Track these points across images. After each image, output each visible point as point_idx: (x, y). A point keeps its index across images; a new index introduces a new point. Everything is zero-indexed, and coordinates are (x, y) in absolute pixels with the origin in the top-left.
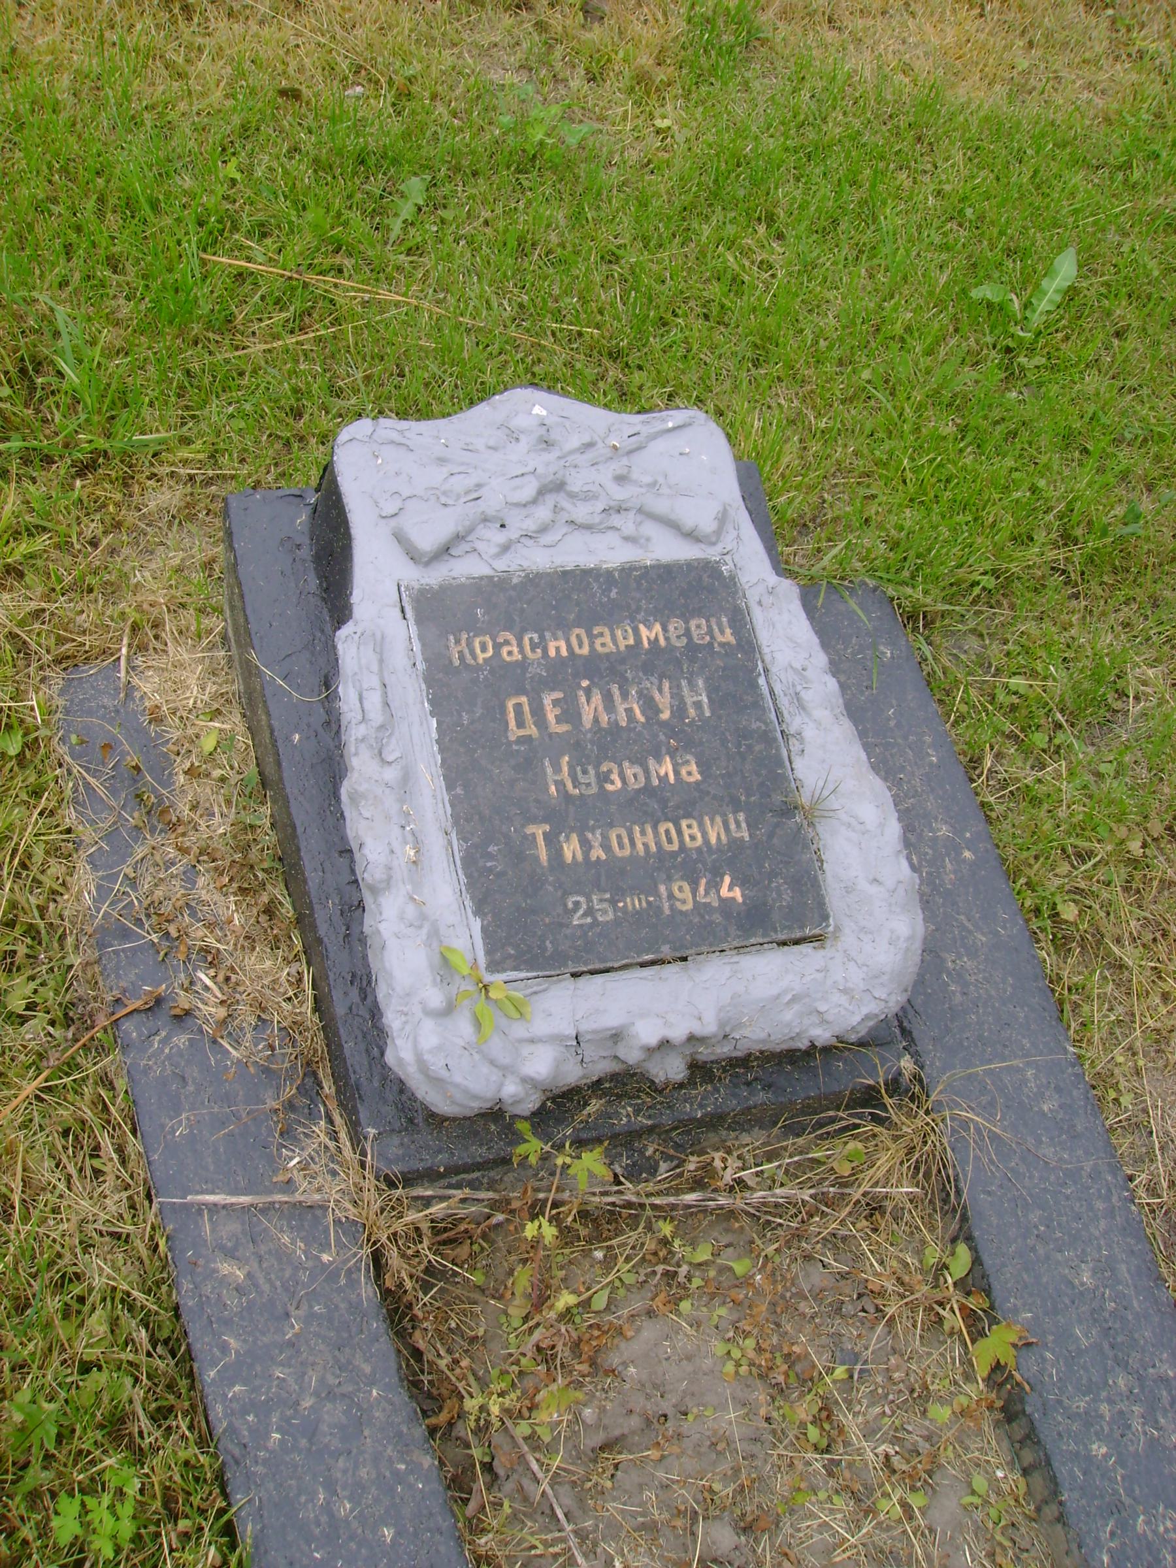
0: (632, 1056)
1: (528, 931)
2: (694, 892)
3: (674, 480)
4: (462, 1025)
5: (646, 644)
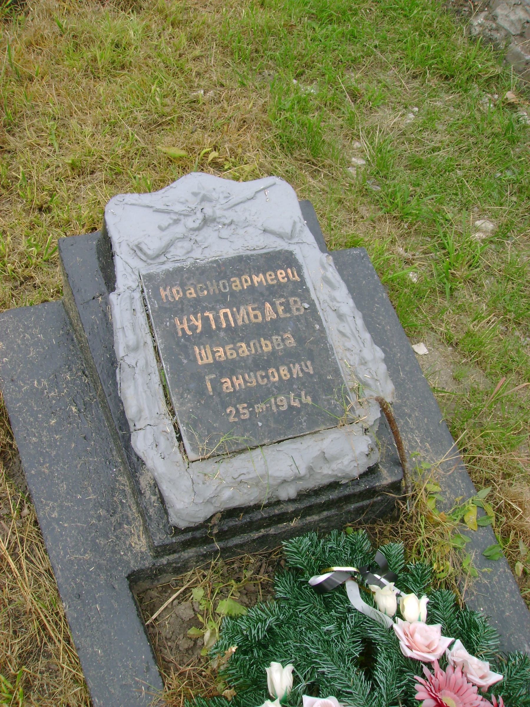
2: (288, 399)
3: (266, 210)
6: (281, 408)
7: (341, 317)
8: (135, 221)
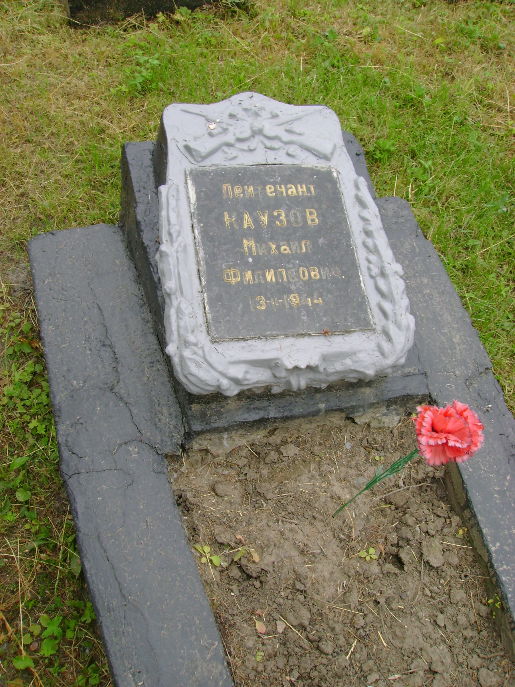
1: (230, 316)
3: (318, 132)
4: (214, 359)
7: (368, 233)
8: (182, 122)
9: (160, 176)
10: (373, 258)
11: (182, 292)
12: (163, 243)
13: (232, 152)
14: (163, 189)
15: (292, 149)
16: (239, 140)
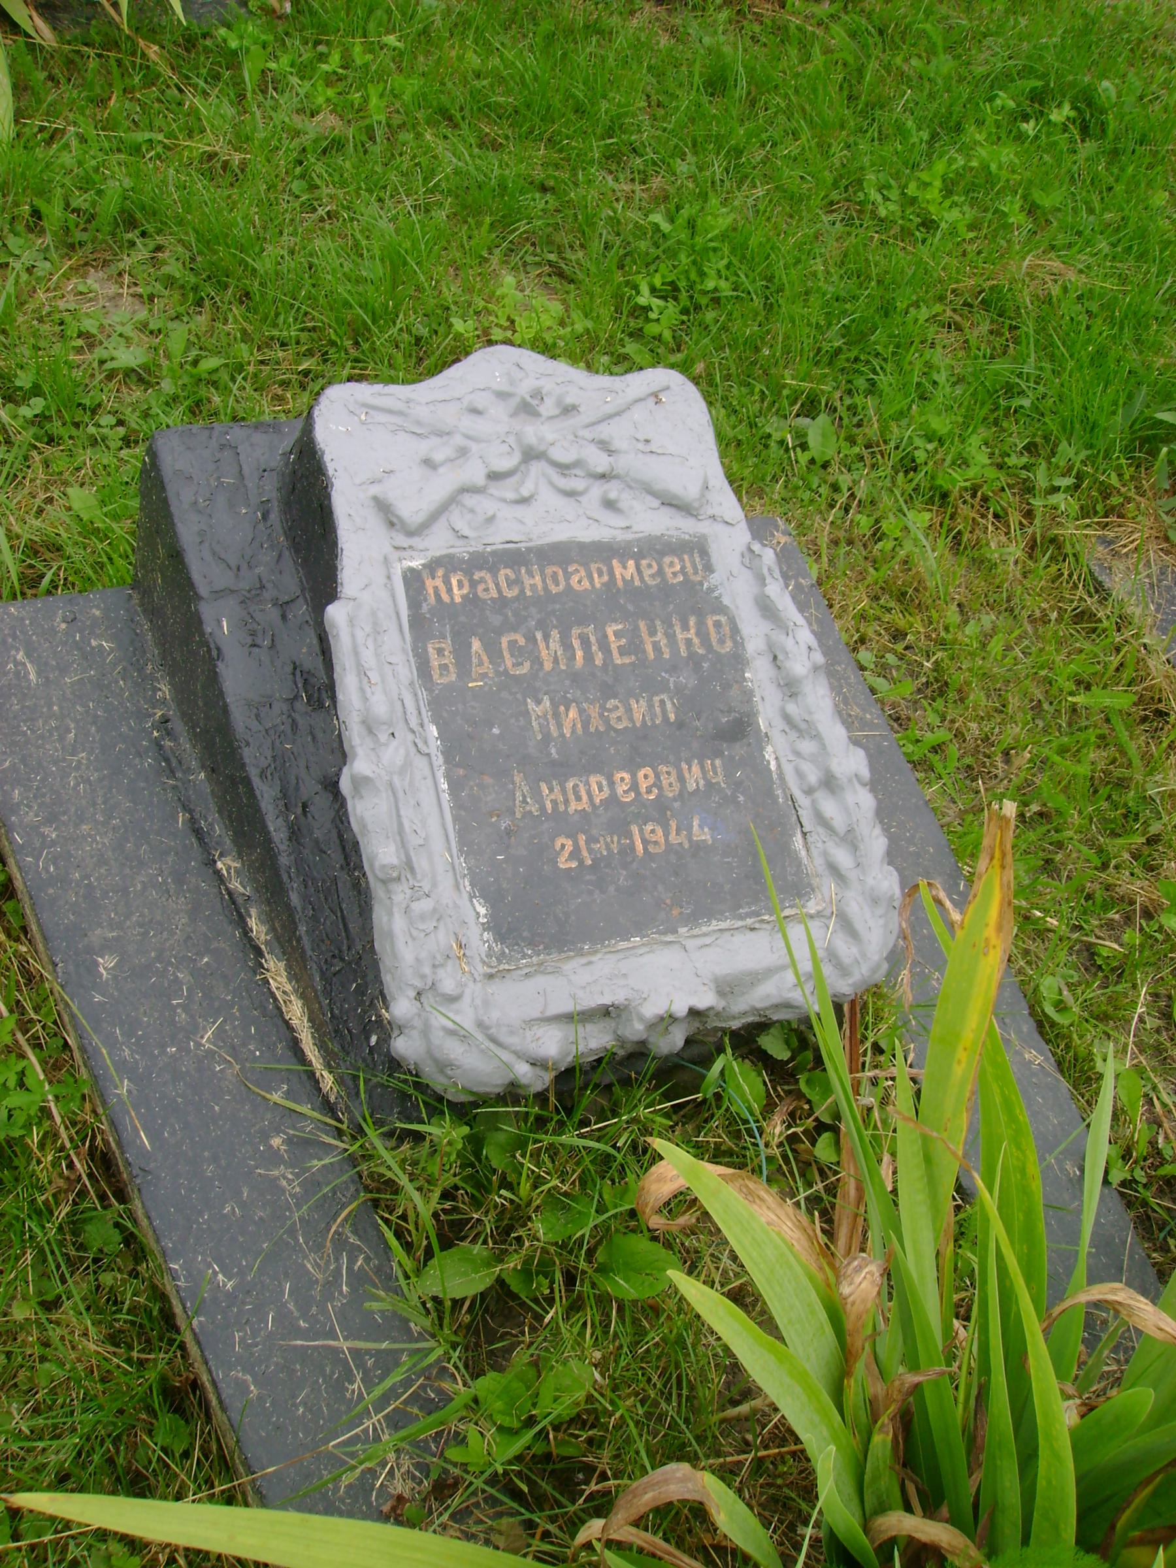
0: (636, 1030)
1: (531, 919)
5: (620, 583)
6: (651, 849)
7: (790, 688)
9: (322, 583)
10: (807, 746)
11: (412, 869)
12: (355, 755)
13: (484, 505)
14: (335, 613)
15: (613, 490)
16: (495, 476)
